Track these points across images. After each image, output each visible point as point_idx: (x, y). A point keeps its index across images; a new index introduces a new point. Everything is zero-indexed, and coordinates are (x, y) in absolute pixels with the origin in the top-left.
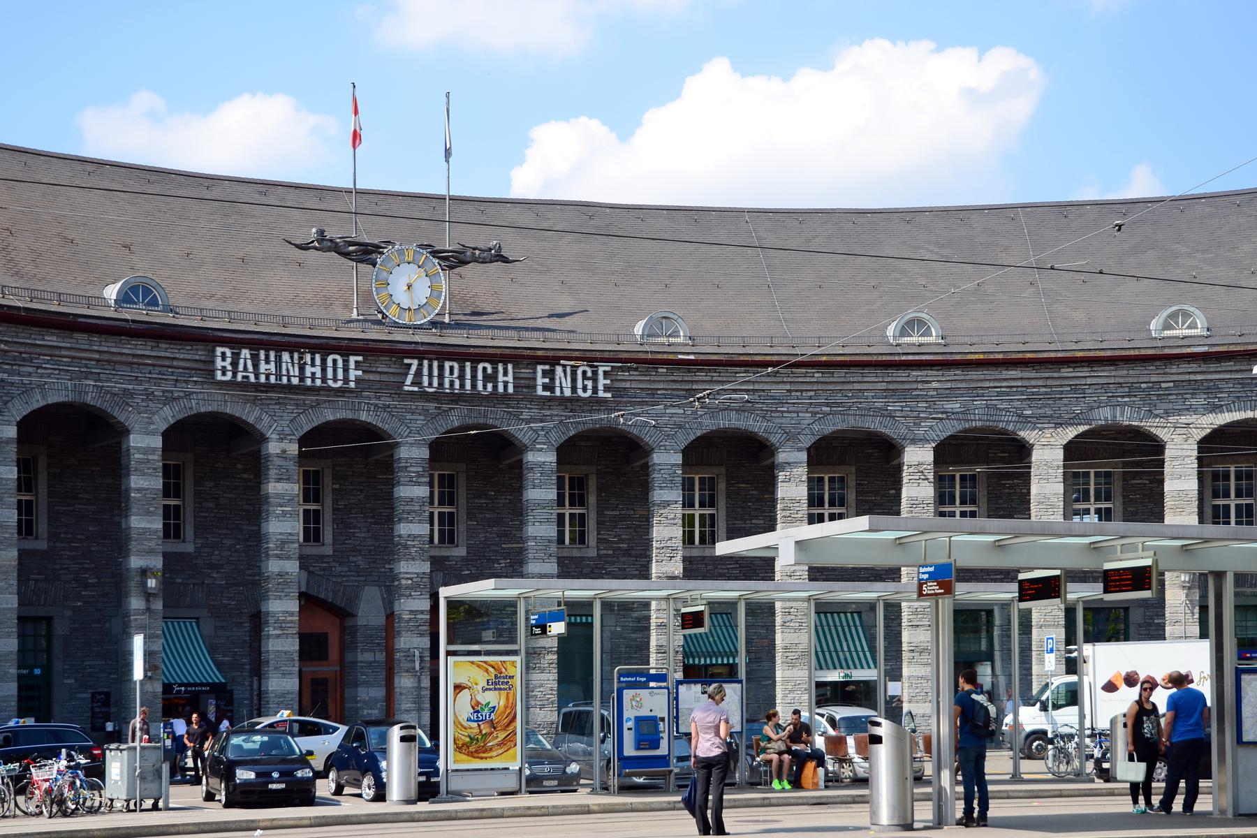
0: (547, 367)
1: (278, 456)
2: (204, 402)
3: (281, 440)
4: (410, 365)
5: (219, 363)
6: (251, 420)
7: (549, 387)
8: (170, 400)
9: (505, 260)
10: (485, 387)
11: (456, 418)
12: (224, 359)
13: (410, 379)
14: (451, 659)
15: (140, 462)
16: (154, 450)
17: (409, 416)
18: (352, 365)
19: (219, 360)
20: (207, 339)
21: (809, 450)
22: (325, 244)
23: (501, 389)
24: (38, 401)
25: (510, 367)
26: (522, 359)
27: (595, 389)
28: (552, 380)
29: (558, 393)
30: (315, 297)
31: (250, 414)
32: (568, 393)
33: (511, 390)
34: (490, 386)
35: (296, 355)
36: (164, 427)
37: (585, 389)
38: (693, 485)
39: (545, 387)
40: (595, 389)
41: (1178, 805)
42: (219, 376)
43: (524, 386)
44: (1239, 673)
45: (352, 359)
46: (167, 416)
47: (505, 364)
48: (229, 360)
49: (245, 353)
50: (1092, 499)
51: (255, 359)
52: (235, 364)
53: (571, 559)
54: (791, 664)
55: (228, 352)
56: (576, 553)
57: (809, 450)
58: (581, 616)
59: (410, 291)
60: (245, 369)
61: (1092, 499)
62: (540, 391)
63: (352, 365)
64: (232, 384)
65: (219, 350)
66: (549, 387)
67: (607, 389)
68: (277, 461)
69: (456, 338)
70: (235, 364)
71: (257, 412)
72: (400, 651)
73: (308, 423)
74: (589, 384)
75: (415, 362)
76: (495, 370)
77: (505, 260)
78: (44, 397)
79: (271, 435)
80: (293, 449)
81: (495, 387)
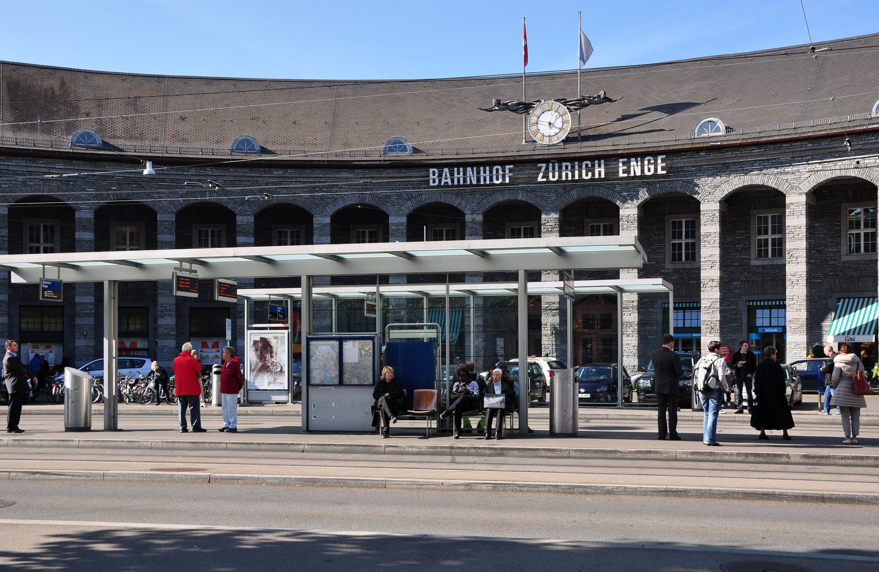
0: (625, 160)
1: (470, 222)
2: (427, 197)
3: (472, 214)
4: (541, 168)
5: (431, 176)
6: (455, 204)
7: (627, 171)
8: (410, 197)
9: (610, 100)
10: (587, 175)
11: (575, 195)
12: (434, 175)
13: (541, 175)
14: (249, 331)
15: (394, 230)
16: (402, 224)
17: (546, 195)
18: (507, 171)
19: (431, 175)
20: (425, 166)
21: (806, 194)
22: (503, 106)
23: (597, 176)
24: (341, 205)
25: (602, 161)
26: (610, 158)
27: (656, 170)
28: (629, 167)
29: (632, 174)
30: (494, 137)
31: (455, 202)
32: (638, 173)
33: (603, 176)
34: (590, 174)
35: (475, 169)
36: (407, 212)
37: (649, 170)
38: (767, 220)
39: (624, 172)
40: (656, 170)
41: (190, 426)
42: (431, 184)
43: (611, 174)
44: (308, 340)
45: (507, 167)
46: (409, 206)
47: (599, 161)
48: (437, 174)
49: (446, 170)
50: (42, 241)
51: (452, 174)
52: (440, 175)
53: (684, 269)
54: (795, 332)
55: (436, 170)
56: (687, 266)
57: (806, 194)
58: (764, 301)
59: (550, 125)
60: (636, 168)
61: (42, 241)
62: (621, 175)
63: (507, 171)
64: (439, 186)
65: (431, 170)
66: (627, 171)
67: (663, 169)
68: (470, 225)
69: (574, 149)
70: (440, 175)
71: (459, 200)
72: (161, 327)
73: (488, 204)
74: (652, 167)
75: (544, 165)
76: (593, 166)
77: (610, 100)
78: (344, 202)
79: (467, 212)
80: (479, 218)
81: (593, 175)
